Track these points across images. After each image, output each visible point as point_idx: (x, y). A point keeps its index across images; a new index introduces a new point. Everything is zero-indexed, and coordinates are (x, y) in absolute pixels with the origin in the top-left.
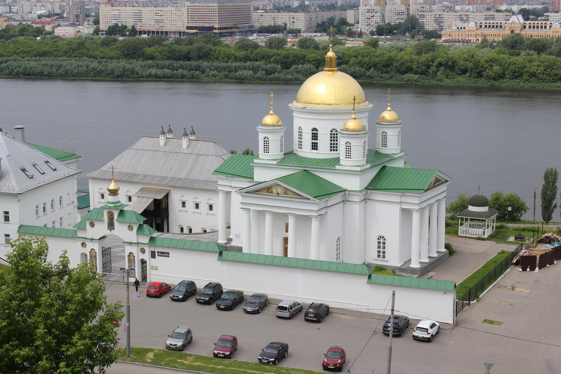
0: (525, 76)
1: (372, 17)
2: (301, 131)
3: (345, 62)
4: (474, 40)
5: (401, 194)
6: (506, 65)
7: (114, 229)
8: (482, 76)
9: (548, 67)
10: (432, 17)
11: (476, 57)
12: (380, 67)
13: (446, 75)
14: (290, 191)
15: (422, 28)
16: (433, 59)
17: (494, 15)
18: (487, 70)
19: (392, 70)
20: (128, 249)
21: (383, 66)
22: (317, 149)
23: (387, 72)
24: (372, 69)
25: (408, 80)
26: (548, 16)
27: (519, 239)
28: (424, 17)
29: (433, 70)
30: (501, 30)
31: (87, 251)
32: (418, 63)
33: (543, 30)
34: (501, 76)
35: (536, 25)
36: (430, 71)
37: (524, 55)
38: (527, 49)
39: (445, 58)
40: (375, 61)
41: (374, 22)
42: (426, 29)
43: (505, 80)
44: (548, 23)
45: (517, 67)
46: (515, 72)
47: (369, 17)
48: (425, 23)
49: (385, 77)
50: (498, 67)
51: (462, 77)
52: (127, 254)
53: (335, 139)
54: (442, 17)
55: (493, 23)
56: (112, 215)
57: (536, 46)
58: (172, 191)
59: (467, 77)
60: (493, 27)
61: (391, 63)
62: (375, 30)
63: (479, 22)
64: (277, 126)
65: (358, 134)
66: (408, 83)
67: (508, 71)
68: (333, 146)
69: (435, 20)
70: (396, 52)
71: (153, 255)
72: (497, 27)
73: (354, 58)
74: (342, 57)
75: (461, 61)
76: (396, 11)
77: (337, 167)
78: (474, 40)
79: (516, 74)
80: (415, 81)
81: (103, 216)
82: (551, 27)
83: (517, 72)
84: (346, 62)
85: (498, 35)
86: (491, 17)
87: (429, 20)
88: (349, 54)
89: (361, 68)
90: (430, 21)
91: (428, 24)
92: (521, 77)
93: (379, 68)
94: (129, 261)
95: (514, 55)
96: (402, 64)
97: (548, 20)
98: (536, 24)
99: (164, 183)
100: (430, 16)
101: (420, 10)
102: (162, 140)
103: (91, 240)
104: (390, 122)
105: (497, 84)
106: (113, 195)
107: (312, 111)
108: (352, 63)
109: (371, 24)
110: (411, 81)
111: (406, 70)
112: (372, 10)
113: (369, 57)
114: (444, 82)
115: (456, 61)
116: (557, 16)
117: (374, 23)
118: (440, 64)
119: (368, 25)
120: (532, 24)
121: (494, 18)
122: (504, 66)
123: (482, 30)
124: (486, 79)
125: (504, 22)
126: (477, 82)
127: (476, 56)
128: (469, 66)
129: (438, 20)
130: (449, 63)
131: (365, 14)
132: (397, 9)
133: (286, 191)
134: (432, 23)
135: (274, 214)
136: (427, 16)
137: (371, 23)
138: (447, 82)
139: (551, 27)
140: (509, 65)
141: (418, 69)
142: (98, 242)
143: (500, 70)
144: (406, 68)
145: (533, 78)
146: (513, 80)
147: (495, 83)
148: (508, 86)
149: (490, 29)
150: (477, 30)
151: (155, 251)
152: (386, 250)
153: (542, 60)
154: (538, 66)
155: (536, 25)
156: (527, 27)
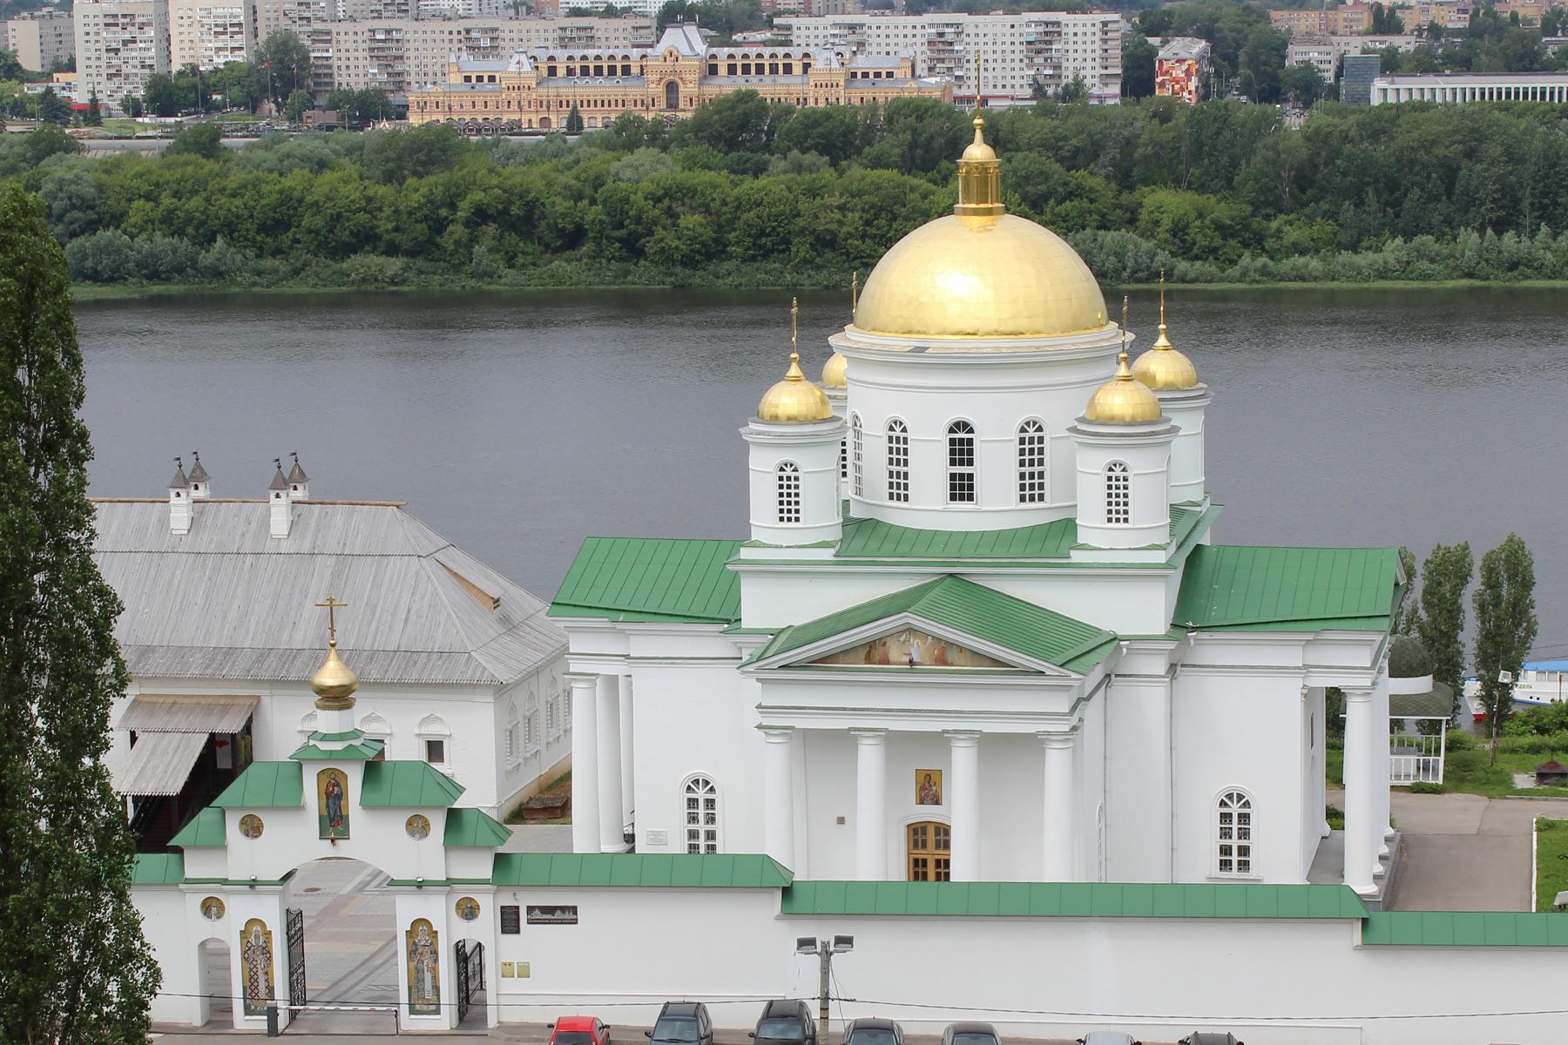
0: (801, 250)
1: (125, 43)
2: (902, 435)
3: (107, 218)
4: (530, 121)
5: (1310, 637)
6: (725, 209)
7: (345, 835)
8: (639, 253)
9: (879, 210)
10: (360, 38)
11: (609, 185)
12: (252, 233)
13: (507, 253)
14: (961, 649)
15: (327, 84)
16: (451, 197)
17: (591, 28)
18: (660, 232)
19: (298, 241)
20: (408, 909)
21: (263, 228)
22: (971, 498)
23: (277, 252)
24: (220, 242)
25: (364, 280)
26: (789, 28)
27: (1553, 780)
28: (329, 41)
29: (456, 236)
30: (630, 82)
31: (229, 930)
32: (397, 211)
33: (781, 78)
34: (713, 251)
35: (753, 62)
36: (447, 241)
37: (785, 172)
38: (789, 149)
39: (497, 191)
40: (229, 210)
41: (136, 62)
42: (340, 84)
43: (727, 266)
44: (796, 53)
45: (769, 215)
46: (762, 233)
47: (114, 45)
48: (336, 63)
49: (276, 271)
50: (698, 218)
51: (566, 261)
52: (403, 926)
53: (1036, 457)
54: (398, 41)
55: (598, 58)
56: (338, 785)
57: (822, 136)
58: (266, 701)
59: (585, 261)
60: (599, 71)
61: (290, 217)
62: (140, 93)
63: (543, 55)
64: (824, 421)
65: (1153, 434)
66: (363, 288)
67: (735, 230)
68: (1027, 481)
69: (372, 50)
70: (306, 172)
71: (509, 921)
72: (612, 70)
73: (142, 202)
74: (94, 199)
75: (558, 200)
76: (211, 21)
77: (1077, 557)
78: (530, 121)
79: (764, 240)
80: (393, 282)
81: (303, 789)
82: (806, 67)
83: (768, 235)
84: (113, 217)
85: (620, 103)
86: (582, 34)
87: (347, 51)
88: (122, 187)
89: (175, 240)
90: (351, 55)
91: (348, 67)
92: (783, 251)
93: (246, 239)
94: (412, 952)
95: (744, 172)
96: (337, 218)
97: (788, 43)
98: (753, 56)
99: (237, 672)
100: (351, 37)
101: (295, 15)
102: (180, 510)
103: (252, 886)
104: (1178, 390)
105: (698, 281)
106: (340, 708)
107: (1002, 361)
108: (140, 222)
109: (125, 70)
110: (376, 280)
111: (354, 240)
112: (124, 16)
113: (204, 194)
114: (503, 281)
115: (538, 200)
116: (821, 28)
117: (135, 67)
118: (481, 215)
119: (114, 75)
120: (739, 57)
121: (592, 38)
122: (718, 214)
123: (559, 84)
124: (657, 263)
125: (636, 53)
126: (625, 277)
127: (611, 179)
128: (589, 217)
129: (379, 49)
130: (514, 210)
131: (97, 34)
132: (214, 11)
133: (944, 652)
134: (361, 62)
135: (893, 741)
136: (342, 38)
137: (124, 66)
138: (509, 280)
139: (806, 67)
140: (738, 208)
141: (398, 238)
142: (279, 892)
143: (701, 225)
144: (352, 232)
145: (829, 255)
146: (757, 265)
147: (690, 277)
148: (741, 284)
149: (587, 79)
150: (538, 84)
151: (518, 908)
152: (1253, 842)
153: (854, 187)
154: (842, 208)
155: (753, 62)
156: (723, 70)
